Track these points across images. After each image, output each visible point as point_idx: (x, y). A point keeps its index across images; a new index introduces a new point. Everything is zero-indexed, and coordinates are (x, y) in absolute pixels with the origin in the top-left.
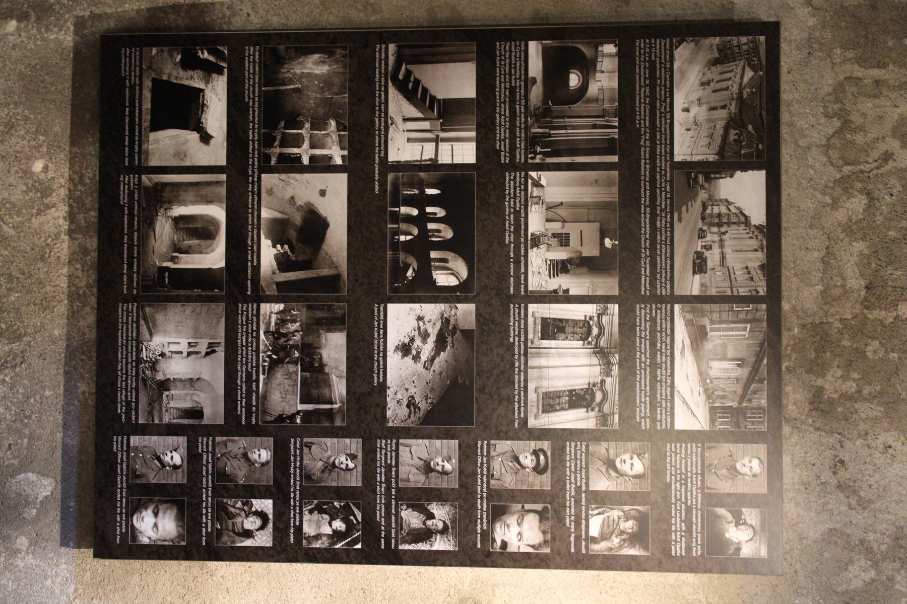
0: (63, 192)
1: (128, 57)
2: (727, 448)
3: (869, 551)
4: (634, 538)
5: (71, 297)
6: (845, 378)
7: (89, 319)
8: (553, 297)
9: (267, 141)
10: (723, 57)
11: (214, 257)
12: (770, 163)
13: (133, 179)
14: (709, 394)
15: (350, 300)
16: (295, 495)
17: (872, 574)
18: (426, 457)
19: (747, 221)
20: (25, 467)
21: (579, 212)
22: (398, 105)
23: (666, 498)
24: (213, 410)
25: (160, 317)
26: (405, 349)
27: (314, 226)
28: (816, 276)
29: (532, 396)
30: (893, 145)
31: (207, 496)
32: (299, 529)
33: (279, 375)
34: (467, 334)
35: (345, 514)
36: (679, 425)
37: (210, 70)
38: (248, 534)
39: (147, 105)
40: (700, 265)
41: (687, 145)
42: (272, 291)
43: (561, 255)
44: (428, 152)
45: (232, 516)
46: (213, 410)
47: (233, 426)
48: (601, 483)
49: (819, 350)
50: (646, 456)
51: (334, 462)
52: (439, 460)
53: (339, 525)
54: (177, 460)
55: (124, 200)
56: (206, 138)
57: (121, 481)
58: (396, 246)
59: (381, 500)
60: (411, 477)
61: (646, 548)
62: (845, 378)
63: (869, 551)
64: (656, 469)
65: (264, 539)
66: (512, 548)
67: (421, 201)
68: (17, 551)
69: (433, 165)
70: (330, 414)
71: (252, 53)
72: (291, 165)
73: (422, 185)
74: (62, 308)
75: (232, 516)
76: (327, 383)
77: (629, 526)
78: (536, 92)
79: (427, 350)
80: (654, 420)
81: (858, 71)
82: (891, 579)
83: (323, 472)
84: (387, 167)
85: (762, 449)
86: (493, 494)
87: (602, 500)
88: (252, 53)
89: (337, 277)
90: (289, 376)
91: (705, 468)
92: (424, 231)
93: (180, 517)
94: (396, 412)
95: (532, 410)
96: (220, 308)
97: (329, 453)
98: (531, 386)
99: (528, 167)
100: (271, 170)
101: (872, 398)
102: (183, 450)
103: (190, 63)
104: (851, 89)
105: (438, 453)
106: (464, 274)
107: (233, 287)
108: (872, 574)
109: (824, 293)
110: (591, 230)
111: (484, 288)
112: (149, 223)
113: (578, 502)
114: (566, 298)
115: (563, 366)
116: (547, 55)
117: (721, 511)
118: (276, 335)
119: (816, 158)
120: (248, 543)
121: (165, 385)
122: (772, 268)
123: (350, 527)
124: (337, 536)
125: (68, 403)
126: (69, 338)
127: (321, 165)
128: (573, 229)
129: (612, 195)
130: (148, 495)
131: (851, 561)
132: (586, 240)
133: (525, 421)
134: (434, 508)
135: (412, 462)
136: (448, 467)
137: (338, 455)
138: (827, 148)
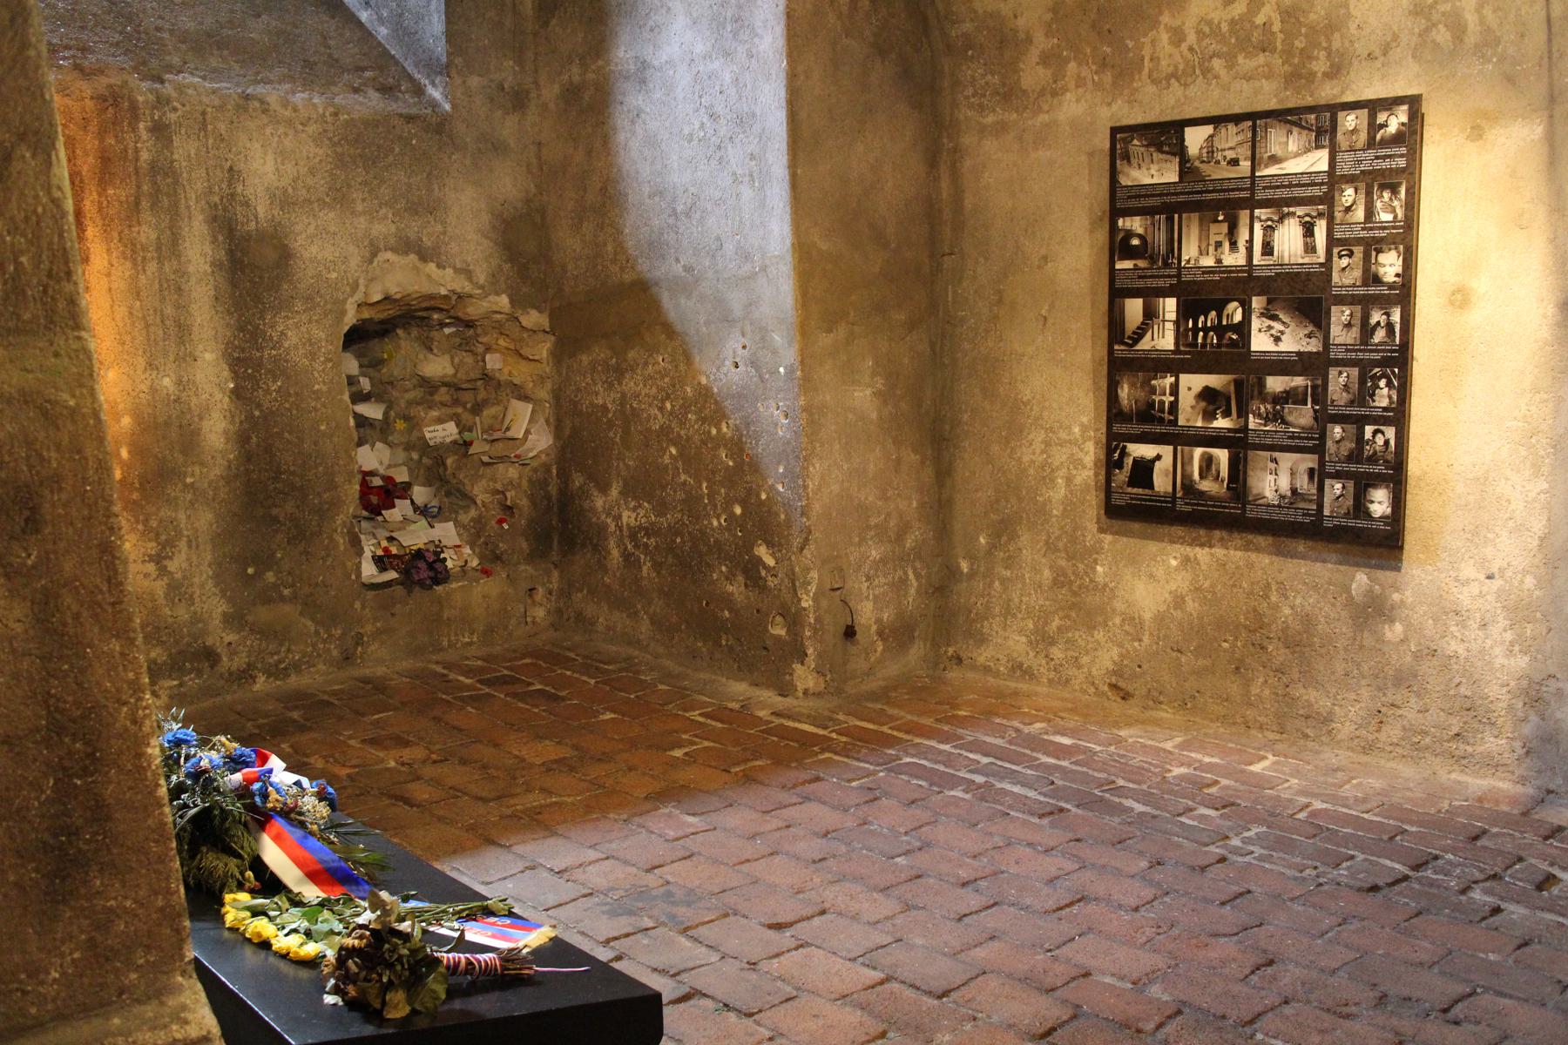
0: (1188, 549)
1: (1118, 500)
2: (1340, 136)
3: (1427, 30)
4: (1394, 190)
5: (1247, 550)
6: (1317, 59)
7: (1262, 540)
8: (1250, 250)
9: (1161, 421)
10: (1127, 157)
11: (1222, 455)
12: (1179, 126)
13: (1179, 502)
14: (1307, 150)
15: (1249, 372)
16: (1363, 411)
17: (1441, 26)
18: (1341, 327)
19: (1211, 136)
20: (1348, 590)
21: (1204, 235)
22: (1145, 344)
23: (1370, 172)
24: (1310, 461)
25: (1255, 491)
26: (1277, 340)
27: (1207, 395)
28: (1257, 84)
29: (1306, 260)
30: (1184, 46)
31: (1363, 468)
32: (1385, 409)
33: (1290, 418)
34: (1269, 302)
35: (1375, 378)
36: (1325, 167)
37: (1124, 453)
38: (1387, 442)
39: (1140, 491)
40: (1234, 162)
41: (1171, 176)
42: (1242, 420)
43: (1227, 245)
44: (1170, 326)
45: (1375, 453)
46: (1310, 461)
47: (1319, 449)
48: (1359, 214)
49: (1300, 76)
53: (1382, 383)
54: (1339, 486)
55: (1189, 509)
56: (1159, 457)
57: (1351, 523)
58: (1219, 345)
59: (1367, 356)
61: (1399, 184)
62: (1317, 59)
63: (1427, 30)
64: (1351, 179)
65: (1390, 432)
66: (1399, 270)
67: (1196, 330)
68: (1402, 601)
69: (1177, 323)
70: (1314, 387)
71: (1117, 428)
72: (1174, 406)
73: (1187, 330)
74: (1253, 556)
75: (1375, 453)
76: (1296, 388)
77: (1386, 195)
78: (1142, 263)
79: (1278, 326)
80: (1322, 184)
81: (1146, 71)
82: (1443, 14)
84: (1176, 351)
85: (1341, 115)
86: (1365, 284)
87: (1370, 213)
88: (1117, 428)
89: (1235, 381)
90: (1290, 412)
91: (1352, 150)
92: (1213, 328)
93: (1375, 486)
94: (1313, 346)
95: (1315, 260)
96: (1250, 453)
98: (1301, 261)
99: (1179, 268)
100: (1176, 419)
101: (1329, 40)
102: (1333, 482)
103: (1119, 464)
104: (1155, 75)
106: (1236, 304)
107: (1238, 443)
108: (1441, 26)
109: (1267, 78)
110: (1214, 228)
111: (1244, 291)
112: (1202, 494)
113: (1371, 229)
114: (1251, 241)
115: (1289, 241)
116: (1121, 259)
117: (1378, 137)
118: (1267, 420)
119: (1193, 91)
120: (1392, 443)
121: (1294, 491)
122: (1236, 119)
123: (1384, 376)
124: (1389, 384)
125: (1310, 559)
126: (1270, 554)
127: (1175, 390)
128: (1213, 239)
129: (1195, 216)
130: (1360, 507)
131: (1433, 41)
132: (1219, 231)
133: (1321, 265)
134: (1373, 321)
137: (1339, 382)
138: (1186, 85)
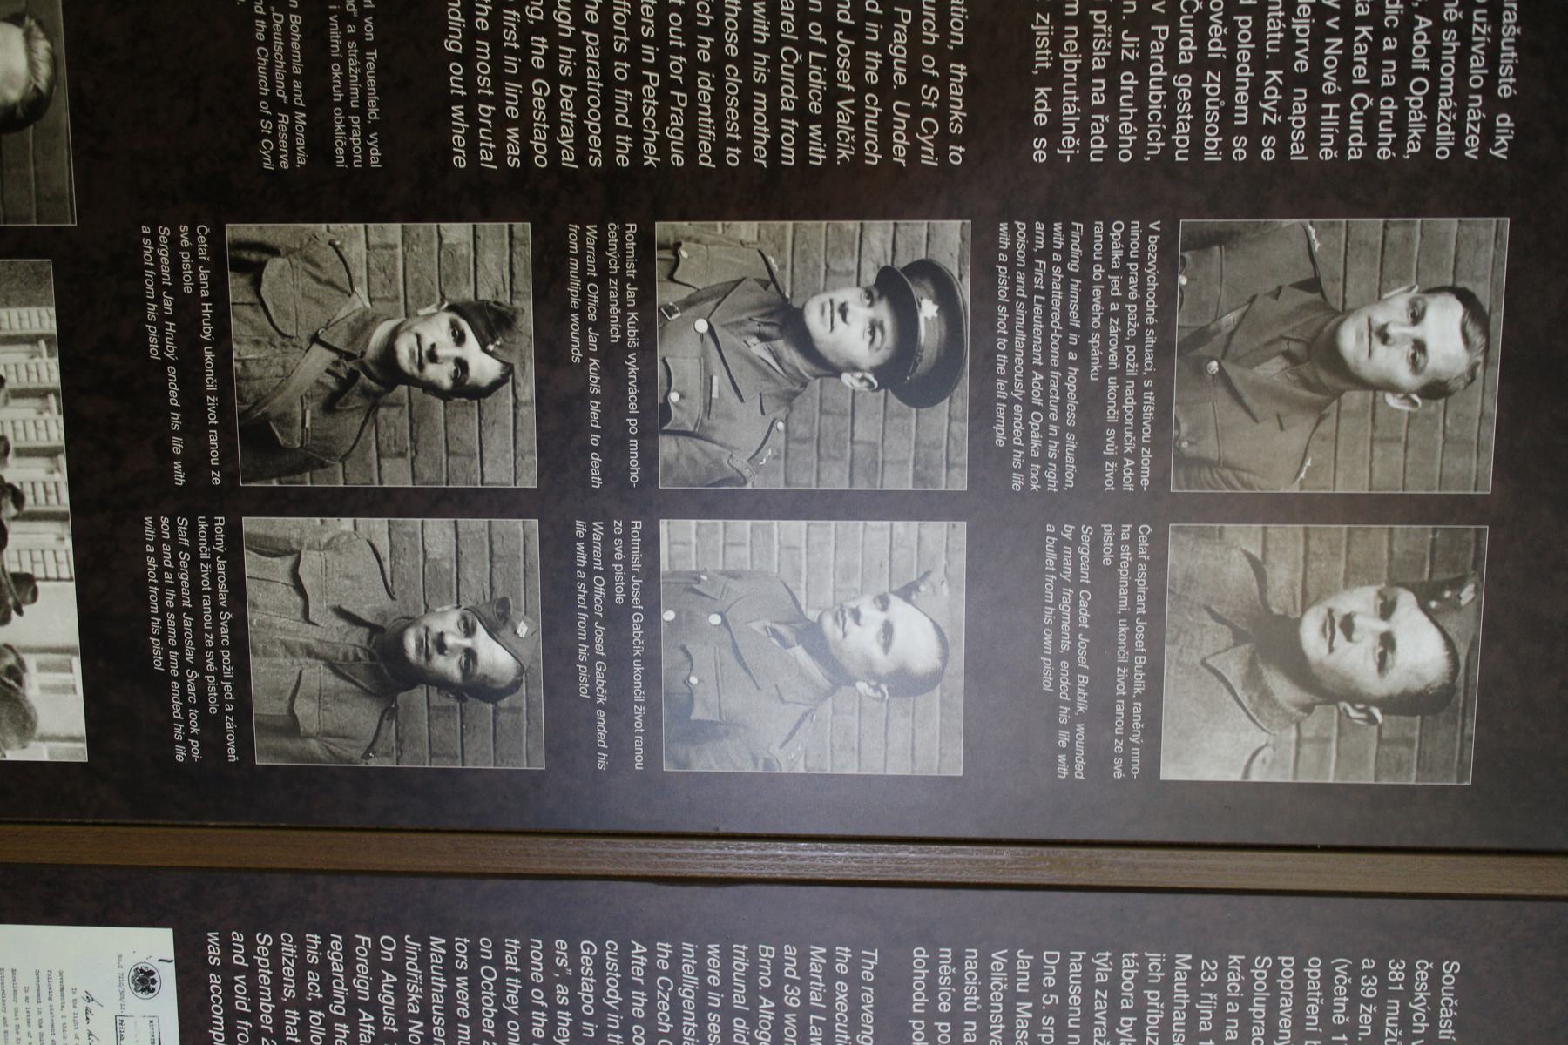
50: (1467, 594)
51: (389, 350)
52: (447, 623)
60: (304, 708)
83: (331, 404)
97: (360, 300)
105: (440, 585)
135: (310, 635)
136: (495, 657)
